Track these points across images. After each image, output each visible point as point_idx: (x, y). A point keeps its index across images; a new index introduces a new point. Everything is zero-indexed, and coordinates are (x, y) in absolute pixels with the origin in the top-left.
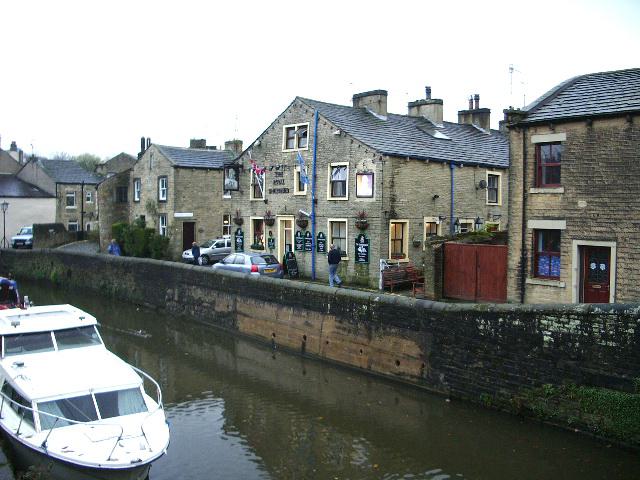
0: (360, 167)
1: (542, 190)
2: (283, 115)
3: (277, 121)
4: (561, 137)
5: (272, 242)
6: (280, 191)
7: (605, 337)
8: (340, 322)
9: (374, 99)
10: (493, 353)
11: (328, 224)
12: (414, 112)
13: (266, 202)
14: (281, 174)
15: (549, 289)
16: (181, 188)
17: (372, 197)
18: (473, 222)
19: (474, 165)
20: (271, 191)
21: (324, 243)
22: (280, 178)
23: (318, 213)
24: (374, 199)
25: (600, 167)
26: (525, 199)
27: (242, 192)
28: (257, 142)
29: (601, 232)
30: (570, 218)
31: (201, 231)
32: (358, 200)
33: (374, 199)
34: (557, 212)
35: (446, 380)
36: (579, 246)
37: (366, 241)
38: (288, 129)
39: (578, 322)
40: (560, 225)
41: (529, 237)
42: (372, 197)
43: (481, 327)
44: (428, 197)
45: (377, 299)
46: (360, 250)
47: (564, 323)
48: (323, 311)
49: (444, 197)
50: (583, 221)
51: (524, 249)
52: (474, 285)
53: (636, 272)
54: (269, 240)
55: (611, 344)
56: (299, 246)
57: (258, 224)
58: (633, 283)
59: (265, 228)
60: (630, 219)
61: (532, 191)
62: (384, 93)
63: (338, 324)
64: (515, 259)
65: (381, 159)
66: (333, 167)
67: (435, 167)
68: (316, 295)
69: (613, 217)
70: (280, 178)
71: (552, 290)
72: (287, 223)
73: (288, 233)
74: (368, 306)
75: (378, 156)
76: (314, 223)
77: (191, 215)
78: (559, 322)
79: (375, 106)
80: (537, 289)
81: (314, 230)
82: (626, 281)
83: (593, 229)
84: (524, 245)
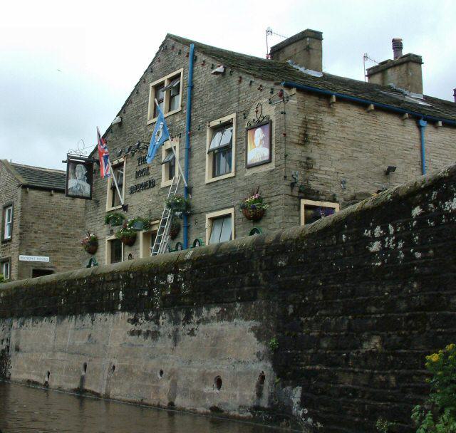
0: (252, 116)
2: (150, 70)
8: (135, 321)
9: (299, 46)
10: (403, 305)
11: (207, 223)
12: (377, 80)
16: (28, 218)
17: (269, 161)
20: (134, 190)
24: (272, 166)
27: (97, 202)
32: (249, 173)
33: (272, 166)
42: (269, 161)
44: (376, 169)
45: (188, 257)
62: (317, 36)
63: (131, 327)
65: (281, 95)
70: (143, 167)
74: (175, 272)
77: (45, 259)
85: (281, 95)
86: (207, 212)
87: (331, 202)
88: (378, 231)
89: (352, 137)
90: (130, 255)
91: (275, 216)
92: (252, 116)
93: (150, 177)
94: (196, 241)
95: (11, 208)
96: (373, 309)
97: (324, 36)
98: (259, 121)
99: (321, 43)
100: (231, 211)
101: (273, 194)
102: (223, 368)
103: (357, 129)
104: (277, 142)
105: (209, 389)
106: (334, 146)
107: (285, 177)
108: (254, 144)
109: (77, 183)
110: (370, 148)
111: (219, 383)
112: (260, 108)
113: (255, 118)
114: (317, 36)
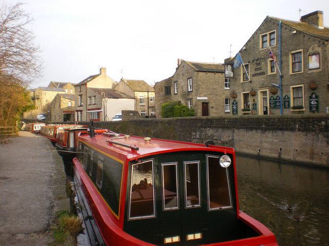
0: (310, 51)
2: (259, 29)
3: (256, 33)
5: (255, 105)
6: (260, 74)
11: (291, 90)
13: (251, 82)
20: (254, 75)
21: (289, 102)
22: (259, 67)
23: (284, 83)
24: (321, 70)
28: (244, 48)
31: (212, 107)
32: (310, 72)
37: (317, 97)
38: (263, 36)
48: (293, 130)
54: (253, 104)
56: (272, 106)
57: (246, 96)
59: (250, 99)
70: (259, 67)
72: (264, 93)
73: (265, 99)
77: (206, 98)
85: (324, 43)
92: (310, 51)
95: (191, 79)
97: (324, 13)
104: (322, 61)
109: (229, 72)
114: (321, 13)
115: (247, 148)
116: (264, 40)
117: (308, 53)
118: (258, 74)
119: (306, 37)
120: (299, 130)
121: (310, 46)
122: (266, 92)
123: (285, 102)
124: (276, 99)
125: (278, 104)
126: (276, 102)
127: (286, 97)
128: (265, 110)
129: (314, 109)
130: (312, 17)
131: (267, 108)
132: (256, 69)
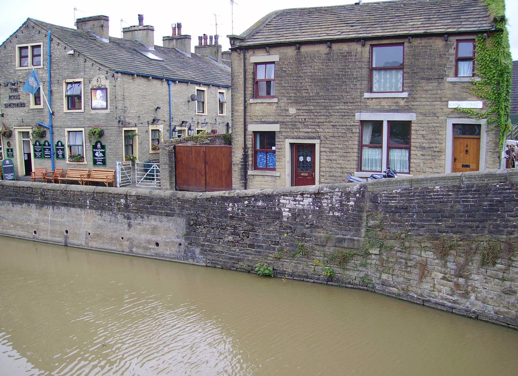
0: (94, 83)
1: (259, 101)
2: (15, 35)
3: (9, 41)
4: (275, 58)
6: (17, 105)
7: (332, 209)
9: (96, 23)
11: (66, 134)
12: (129, 36)
14: (16, 90)
15: (267, 178)
18: (186, 129)
19: (186, 82)
21: (63, 150)
22: (15, 94)
23: (55, 124)
24: (108, 111)
25: (307, 82)
26: (245, 107)
29: (308, 132)
30: (283, 122)
32: (93, 112)
33: (108, 111)
34: (272, 117)
35: (201, 253)
36: (292, 145)
37: (103, 147)
38: (21, 48)
39: (311, 199)
40: (275, 128)
41: (250, 138)
42: (107, 108)
43: (230, 209)
44: (152, 108)
46: (97, 154)
47: (299, 201)
48: (82, 206)
49: (165, 108)
50: (294, 125)
51: (245, 148)
52: (203, 178)
53: (335, 162)
54: (8, 150)
55: (336, 214)
58: (333, 170)
60: (330, 122)
61: (251, 101)
63: (100, 217)
64: (237, 156)
66: (68, 83)
67: (156, 83)
68: (74, 194)
69: (317, 120)
70: (15, 94)
71: (269, 179)
74: (126, 199)
75: (110, 74)
76: (52, 133)
78: (295, 200)
79: (98, 30)
80: (257, 178)
81: (52, 139)
82: (328, 169)
83: (301, 130)
84: (245, 145)
85: (113, 76)
86: (66, 127)
87: (134, 127)
88: (231, 204)
89: (142, 94)
90: (8, 142)
91: (111, 136)
93: (21, 101)
94: (58, 142)
96: (229, 228)
98: (99, 86)
99: (108, 23)
100: (83, 129)
101: (109, 125)
102: (159, 239)
103: (144, 89)
105: (153, 246)
106: (135, 99)
107: (116, 118)
108: (96, 98)
110: (149, 98)
111: (157, 244)
112: (99, 80)
113: (96, 84)
115: (15, 228)
116: (23, 54)
117: (91, 85)
118: (14, 104)
119: (87, 63)
120: (91, 208)
121: (94, 76)
122: (28, 133)
123: (57, 149)
124: (45, 145)
125: (47, 152)
126: (45, 149)
127: (60, 144)
128: (26, 158)
129: (99, 163)
130: (91, 23)
131: (29, 155)
132: (10, 97)
